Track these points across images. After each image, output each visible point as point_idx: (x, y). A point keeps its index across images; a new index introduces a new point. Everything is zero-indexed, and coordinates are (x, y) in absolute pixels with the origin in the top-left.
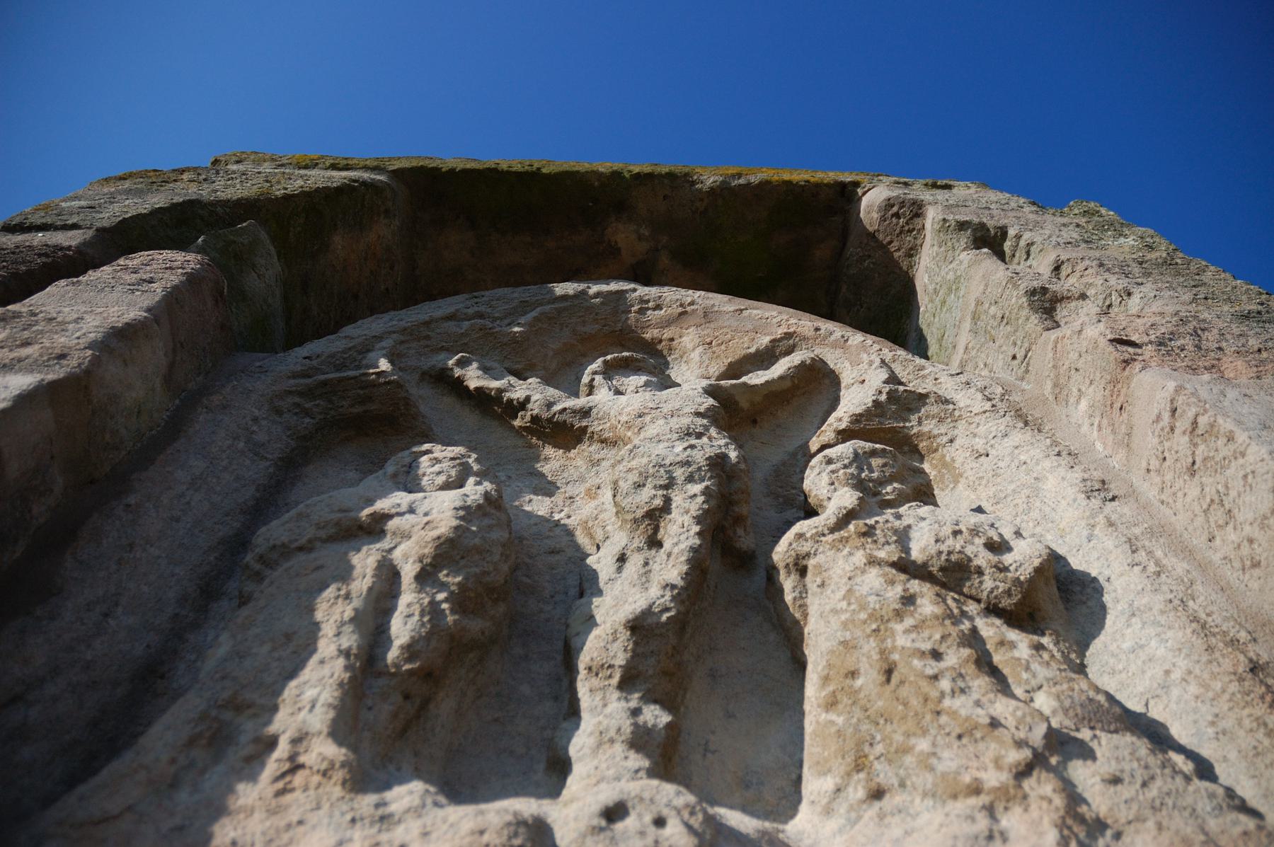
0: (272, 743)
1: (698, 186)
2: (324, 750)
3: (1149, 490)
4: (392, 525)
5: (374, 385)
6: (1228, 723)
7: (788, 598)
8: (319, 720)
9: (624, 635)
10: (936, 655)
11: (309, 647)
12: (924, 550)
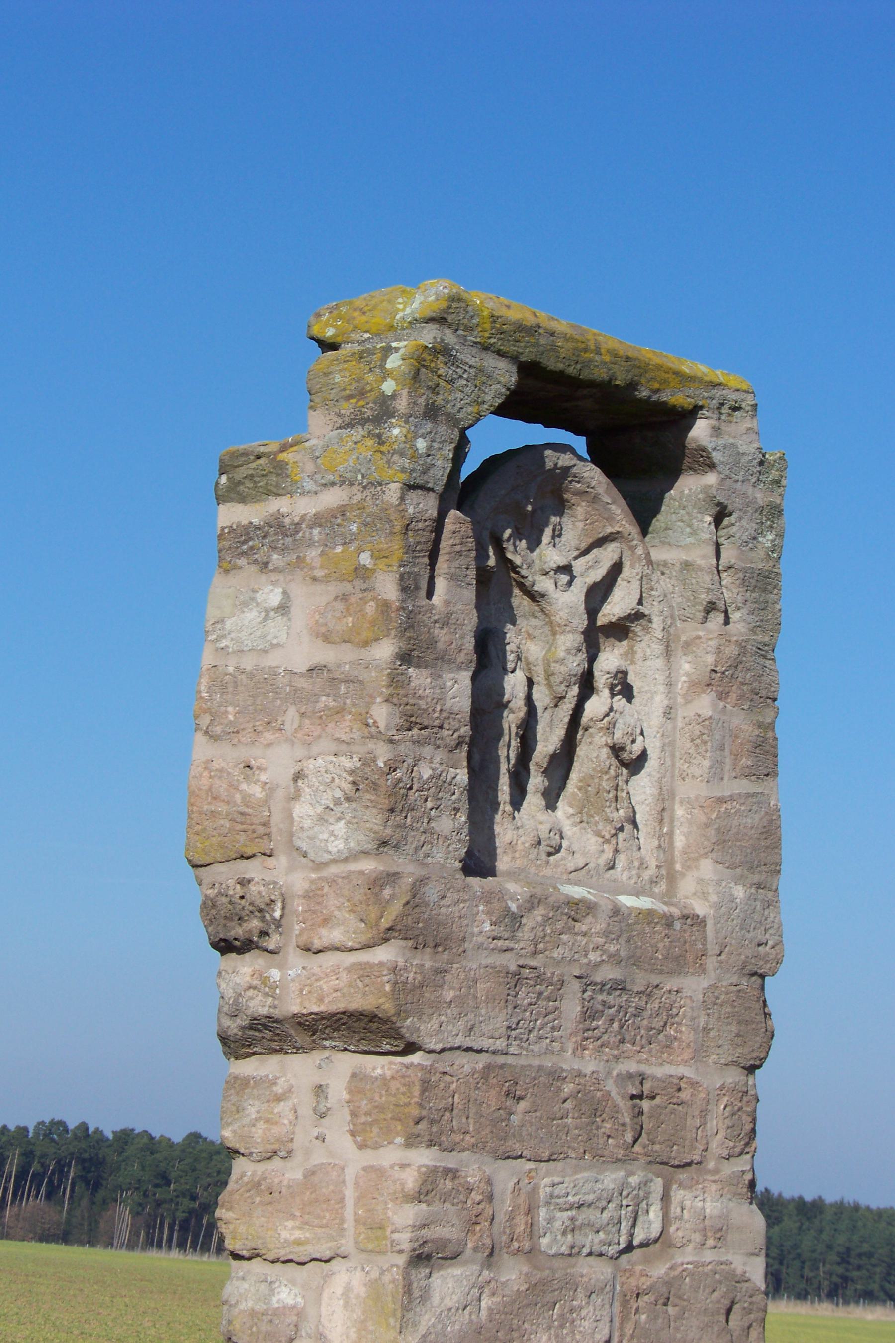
1: (637, 393)
3: (680, 723)
6: (649, 823)
9: (548, 757)
12: (618, 739)
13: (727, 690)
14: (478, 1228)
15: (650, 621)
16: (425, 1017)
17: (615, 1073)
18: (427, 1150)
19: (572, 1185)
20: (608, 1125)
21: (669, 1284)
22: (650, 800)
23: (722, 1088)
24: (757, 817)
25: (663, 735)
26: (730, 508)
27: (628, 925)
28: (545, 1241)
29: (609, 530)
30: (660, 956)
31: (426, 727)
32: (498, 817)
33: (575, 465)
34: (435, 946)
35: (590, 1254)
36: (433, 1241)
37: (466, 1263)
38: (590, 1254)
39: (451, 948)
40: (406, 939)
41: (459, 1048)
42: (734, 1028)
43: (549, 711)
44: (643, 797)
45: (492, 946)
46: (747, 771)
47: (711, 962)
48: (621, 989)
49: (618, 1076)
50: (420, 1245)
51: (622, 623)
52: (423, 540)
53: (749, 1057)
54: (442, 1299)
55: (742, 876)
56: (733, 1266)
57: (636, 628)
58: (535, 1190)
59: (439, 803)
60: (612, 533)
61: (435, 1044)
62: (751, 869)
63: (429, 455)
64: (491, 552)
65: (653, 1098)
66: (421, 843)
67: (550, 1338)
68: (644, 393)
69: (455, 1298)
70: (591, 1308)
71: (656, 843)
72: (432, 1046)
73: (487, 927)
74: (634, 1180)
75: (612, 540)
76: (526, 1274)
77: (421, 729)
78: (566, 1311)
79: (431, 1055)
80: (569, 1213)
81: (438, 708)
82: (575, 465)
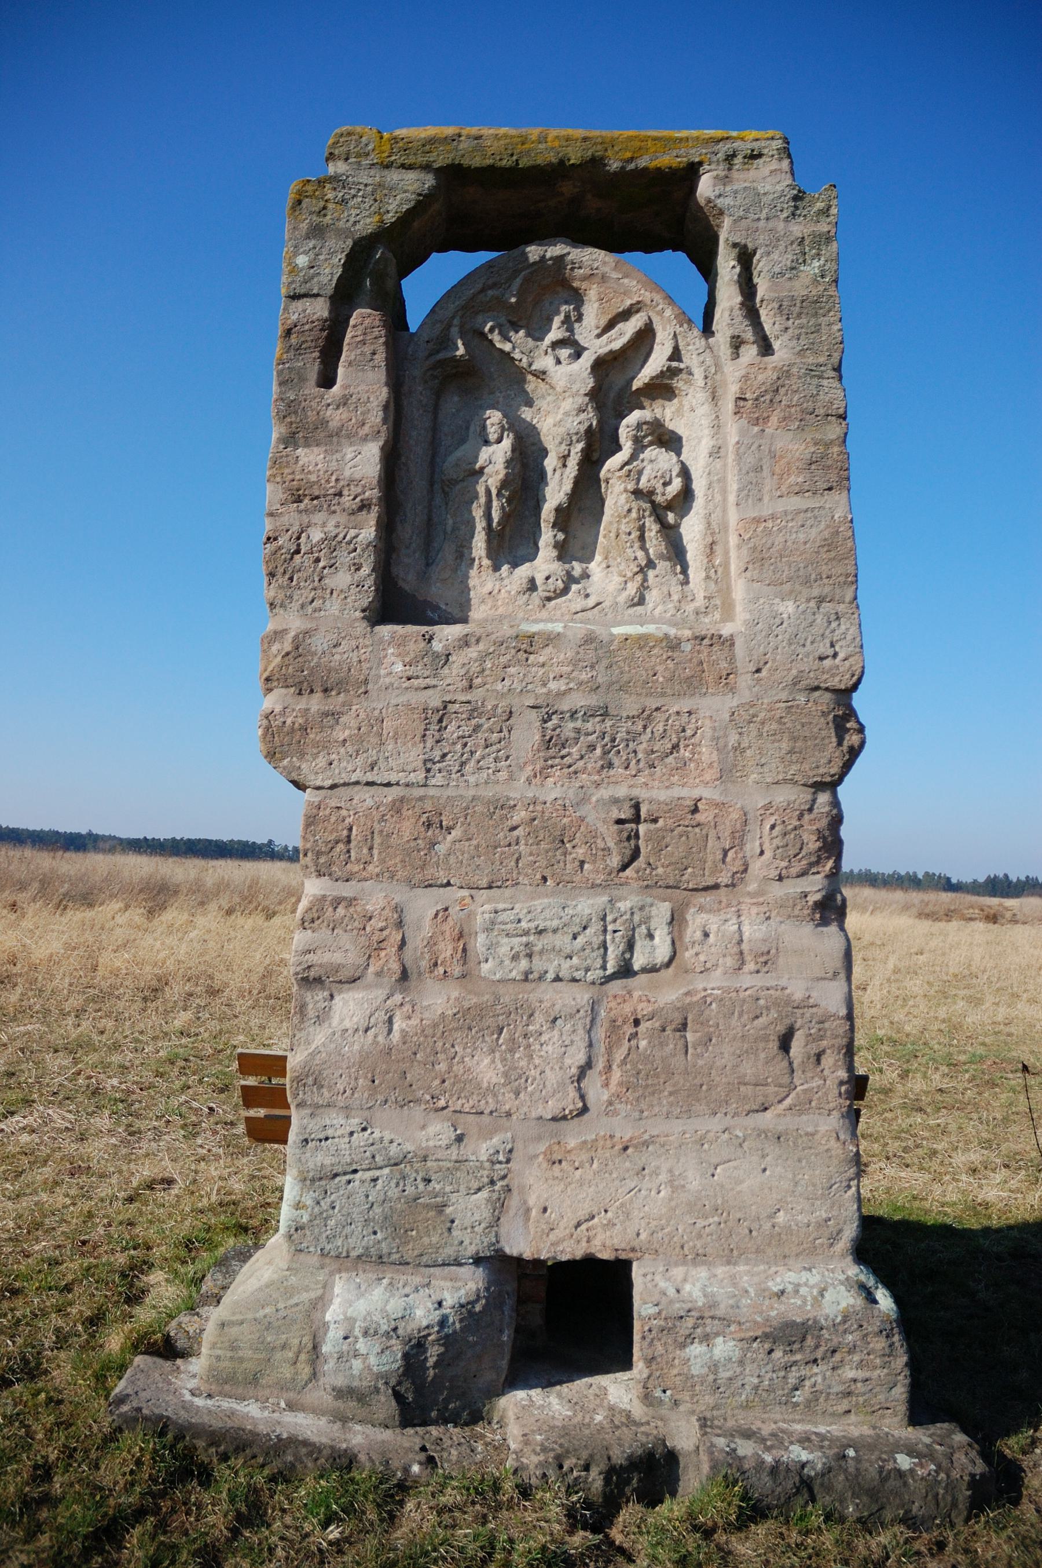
0: (474, 560)
1: (608, 168)
2: (486, 562)
4: (486, 470)
5: (459, 360)
7: (603, 490)
8: (483, 553)
9: (553, 512)
10: (630, 534)
11: (474, 528)
13: (765, 415)
14: (383, 954)
15: (691, 374)
16: (308, 757)
17: (594, 799)
18: (318, 880)
19: (525, 911)
20: (581, 851)
21: (684, 1009)
22: (698, 536)
23: (768, 807)
24: (814, 531)
25: (709, 474)
26: (750, 246)
27: (609, 651)
28: (485, 967)
29: (628, 302)
30: (661, 679)
31: (317, 498)
32: (473, 573)
33: (569, 253)
34: (326, 691)
35: (558, 979)
36: (321, 965)
37: (368, 987)
38: (558, 979)
39: (347, 691)
40: (287, 687)
41: (357, 783)
42: (785, 745)
43: (558, 473)
44: (693, 535)
45: (404, 685)
46: (797, 488)
47: (744, 681)
48: (601, 715)
49: (598, 801)
50: (304, 970)
51: (658, 381)
52: (309, 339)
53: (811, 774)
54: (342, 1020)
55: (791, 592)
56: (788, 991)
57: (678, 383)
58: (471, 916)
59: (333, 561)
60: (632, 305)
61: (323, 780)
62: (807, 582)
63: (313, 267)
64: (460, 343)
65: (655, 821)
66: (310, 599)
67: (493, 1061)
68: (614, 166)
69: (355, 1019)
70: (556, 1033)
71: (704, 574)
72: (318, 783)
73: (399, 667)
74: (623, 906)
75: (638, 311)
76: (457, 999)
77: (312, 499)
78: (517, 1035)
79: (320, 791)
80: (524, 939)
81: (334, 478)
82: (569, 253)
